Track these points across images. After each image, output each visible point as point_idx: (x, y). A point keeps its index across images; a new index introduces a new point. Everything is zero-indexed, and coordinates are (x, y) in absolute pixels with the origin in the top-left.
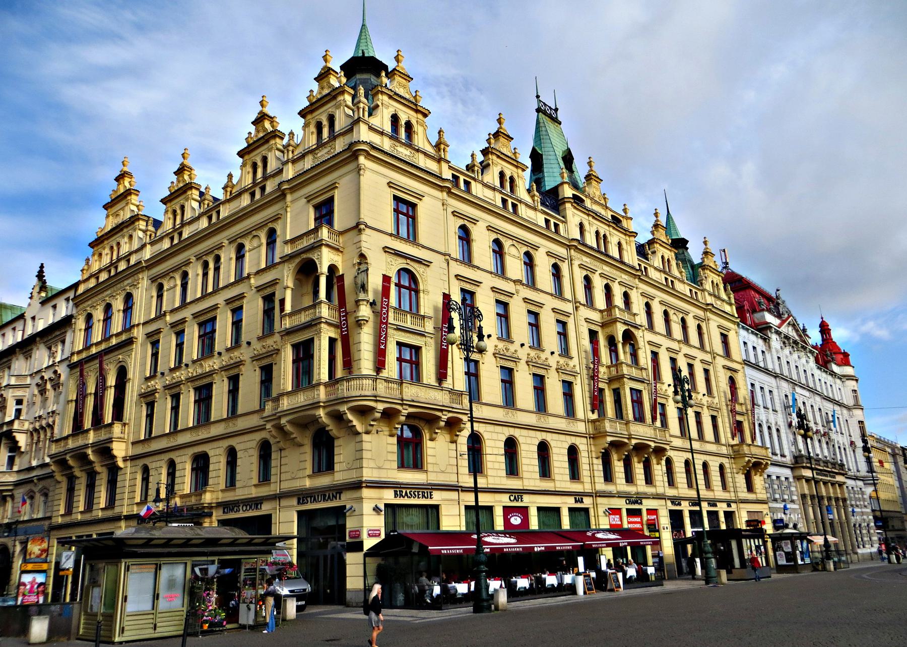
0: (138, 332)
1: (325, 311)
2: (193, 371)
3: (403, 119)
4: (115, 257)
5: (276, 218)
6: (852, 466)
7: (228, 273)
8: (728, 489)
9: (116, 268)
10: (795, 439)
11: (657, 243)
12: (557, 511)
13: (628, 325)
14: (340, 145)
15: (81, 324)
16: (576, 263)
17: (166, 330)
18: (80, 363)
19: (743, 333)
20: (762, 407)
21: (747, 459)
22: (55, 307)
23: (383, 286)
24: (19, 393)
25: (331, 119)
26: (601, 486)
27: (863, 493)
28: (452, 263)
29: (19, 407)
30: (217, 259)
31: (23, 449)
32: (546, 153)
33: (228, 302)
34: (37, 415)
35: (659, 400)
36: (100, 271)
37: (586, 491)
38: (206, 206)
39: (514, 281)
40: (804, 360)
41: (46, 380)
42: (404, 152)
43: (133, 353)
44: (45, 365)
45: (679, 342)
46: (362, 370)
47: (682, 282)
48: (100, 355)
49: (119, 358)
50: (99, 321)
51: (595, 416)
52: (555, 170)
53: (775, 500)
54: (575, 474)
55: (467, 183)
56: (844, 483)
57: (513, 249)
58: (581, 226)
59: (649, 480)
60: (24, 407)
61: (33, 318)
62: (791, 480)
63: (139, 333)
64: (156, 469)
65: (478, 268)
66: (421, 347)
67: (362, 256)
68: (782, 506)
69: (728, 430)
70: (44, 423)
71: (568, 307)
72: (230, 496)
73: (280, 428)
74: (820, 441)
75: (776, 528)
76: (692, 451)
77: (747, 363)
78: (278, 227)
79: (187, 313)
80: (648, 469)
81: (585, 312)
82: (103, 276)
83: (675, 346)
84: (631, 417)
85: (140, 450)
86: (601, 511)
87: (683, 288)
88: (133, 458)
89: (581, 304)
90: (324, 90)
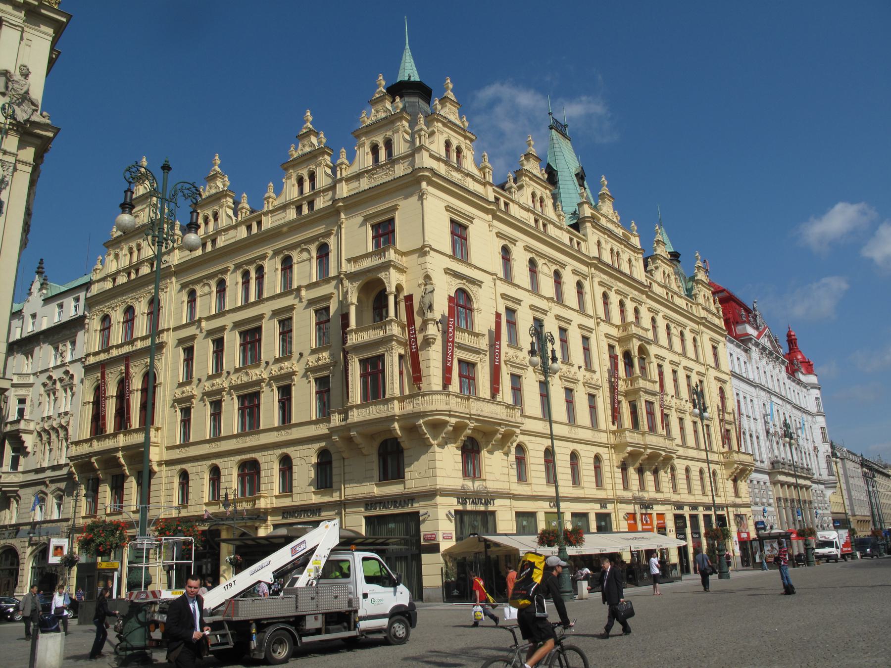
0: (168, 336)
1: (395, 330)
2: (235, 379)
3: (455, 143)
4: (135, 259)
5: (328, 234)
6: (815, 471)
7: (273, 282)
8: (647, 489)
9: (137, 271)
10: (771, 445)
11: (659, 259)
12: (532, 515)
13: (642, 340)
14: (401, 170)
15: (95, 324)
16: (596, 280)
17: (201, 336)
18: (102, 366)
19: (730, 345)
20: (745, 416)
21: (736, 465)
22: (61, 306)
23: (449, 307)
24: (22, 392)
25: (389, 144)
26: (621, 493)
27: (824, 496)
28: (498, 282)
29: (22, 406)
30: (260, 270)
31: (29, 450)
32: (561, 170)
33: (275, 313)
34: (45, 415)
35: (459, 354)
36: (118, 272)
37: (609, 497)
38: (244, 215)
39: (548, 299)
40: (777, 370)
41: (55, 380)
42: (456, 176)
43: (163, 358)
44: (52, 365)
45: (679, 354)
46: (433, 385)
47: (681, 297)
48: (126, 359)
49: (147, 362)
50: (119, 322)
51: (615, 428)
52: (570, 187)
53: (756, 504)
54: (599, 483)
55: (506, 204)
56: (811, 486)
57: (545, 267)
58: (599, 243)
59: (658, 488)
60: (27, 407)
61: (34, 316)
62: (768, 484)
63: (170, 338)
64: (197, 474)
65: (519, 287)
66: (477, 363)
67: (427, 277)
68: (761, 508)
69: (720, 438)
70: (55, 424)
71: (590, 323)
72: (286, 502)
73: (350, 440)
74: (778, 443)
75: (757, 529)
76: (552, 437)
77: (734, 375)
78: (332, 242)
79: (227, 321)
80: (551, 465)
81: (604, 328)
82: (122, 279)
83: (676, 358)
84: (646, 429)
85: (176, 454)
86: (621, 515)
87: (681, 302)
88: (169, 463)
89: (601, 320)
90: (380, 113)
